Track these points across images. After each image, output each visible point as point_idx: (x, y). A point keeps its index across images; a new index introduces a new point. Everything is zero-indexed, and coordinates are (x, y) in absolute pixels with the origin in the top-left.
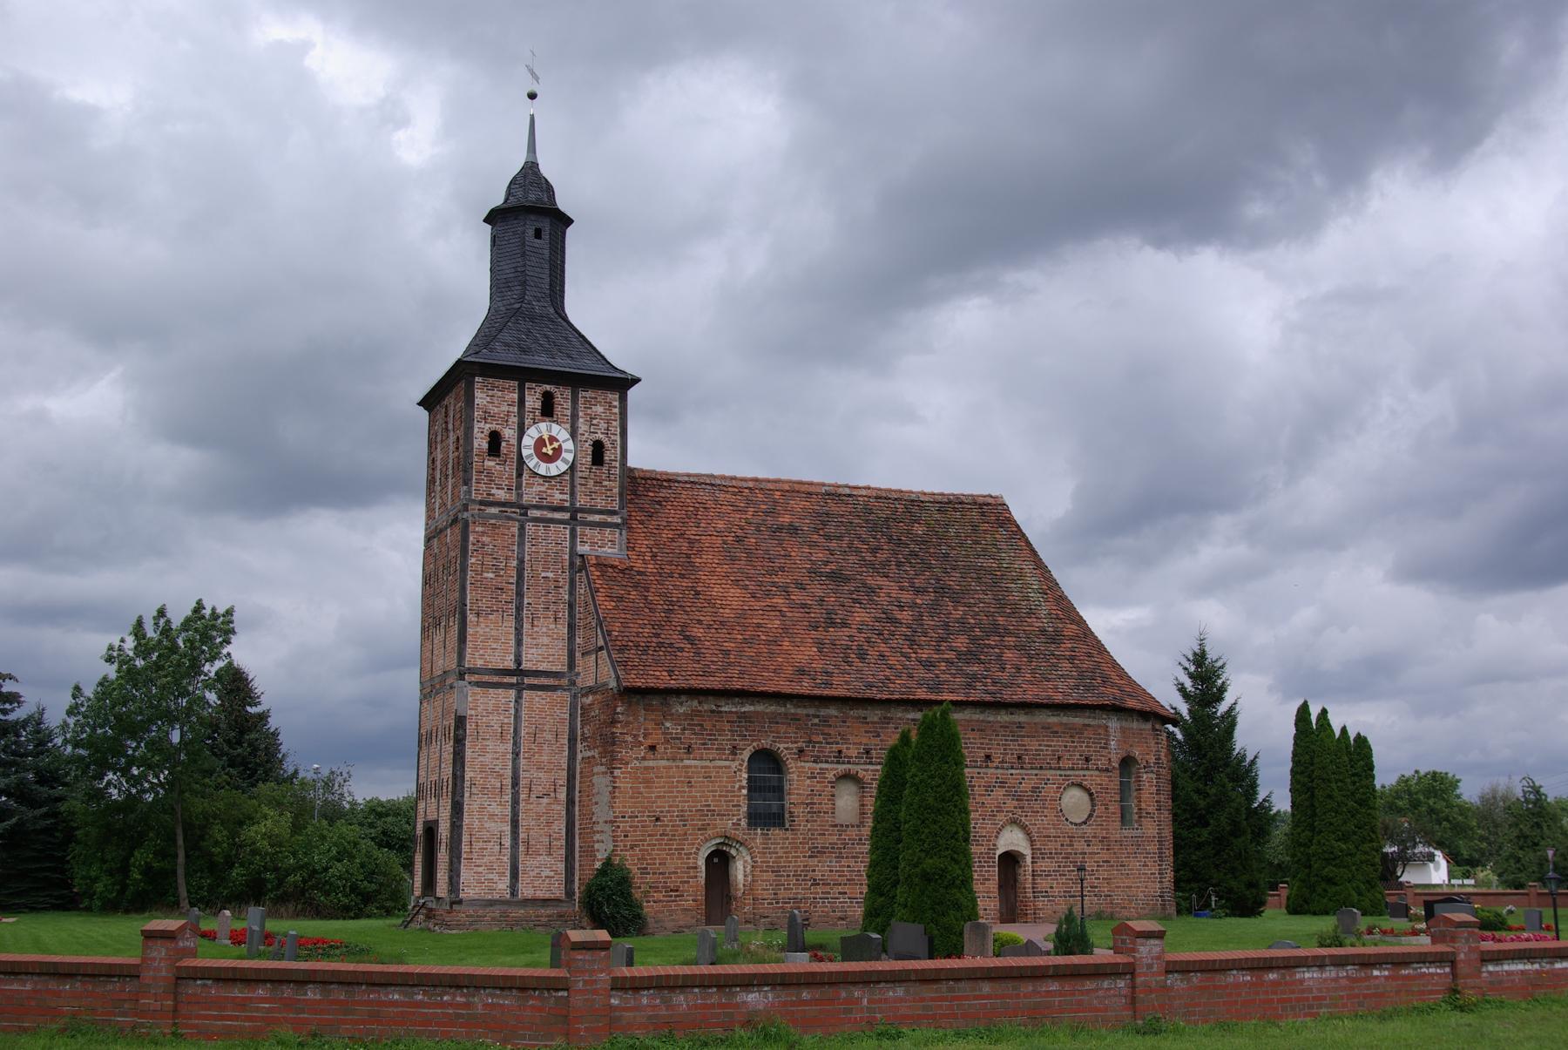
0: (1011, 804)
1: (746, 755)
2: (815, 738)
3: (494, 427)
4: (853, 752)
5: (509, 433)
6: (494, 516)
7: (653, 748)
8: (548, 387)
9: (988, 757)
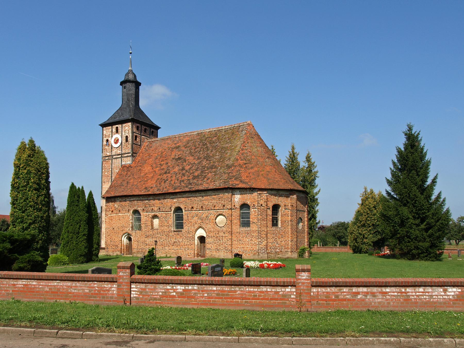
0: (199, 221)
1: (131, 211)
2: (147, 206)
3: (107, 138)
4: (156, 209)
5: (109, 139)
6: (108, 159)
7: (112, 211)
8: (117, 126)
9: (192, 208)
